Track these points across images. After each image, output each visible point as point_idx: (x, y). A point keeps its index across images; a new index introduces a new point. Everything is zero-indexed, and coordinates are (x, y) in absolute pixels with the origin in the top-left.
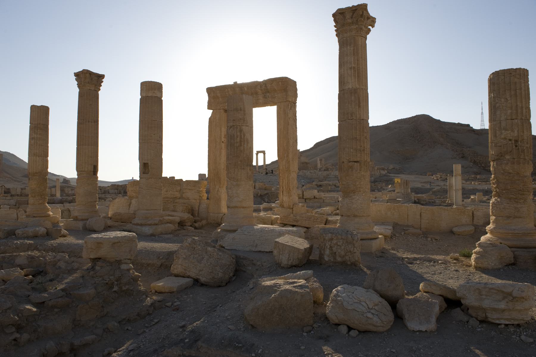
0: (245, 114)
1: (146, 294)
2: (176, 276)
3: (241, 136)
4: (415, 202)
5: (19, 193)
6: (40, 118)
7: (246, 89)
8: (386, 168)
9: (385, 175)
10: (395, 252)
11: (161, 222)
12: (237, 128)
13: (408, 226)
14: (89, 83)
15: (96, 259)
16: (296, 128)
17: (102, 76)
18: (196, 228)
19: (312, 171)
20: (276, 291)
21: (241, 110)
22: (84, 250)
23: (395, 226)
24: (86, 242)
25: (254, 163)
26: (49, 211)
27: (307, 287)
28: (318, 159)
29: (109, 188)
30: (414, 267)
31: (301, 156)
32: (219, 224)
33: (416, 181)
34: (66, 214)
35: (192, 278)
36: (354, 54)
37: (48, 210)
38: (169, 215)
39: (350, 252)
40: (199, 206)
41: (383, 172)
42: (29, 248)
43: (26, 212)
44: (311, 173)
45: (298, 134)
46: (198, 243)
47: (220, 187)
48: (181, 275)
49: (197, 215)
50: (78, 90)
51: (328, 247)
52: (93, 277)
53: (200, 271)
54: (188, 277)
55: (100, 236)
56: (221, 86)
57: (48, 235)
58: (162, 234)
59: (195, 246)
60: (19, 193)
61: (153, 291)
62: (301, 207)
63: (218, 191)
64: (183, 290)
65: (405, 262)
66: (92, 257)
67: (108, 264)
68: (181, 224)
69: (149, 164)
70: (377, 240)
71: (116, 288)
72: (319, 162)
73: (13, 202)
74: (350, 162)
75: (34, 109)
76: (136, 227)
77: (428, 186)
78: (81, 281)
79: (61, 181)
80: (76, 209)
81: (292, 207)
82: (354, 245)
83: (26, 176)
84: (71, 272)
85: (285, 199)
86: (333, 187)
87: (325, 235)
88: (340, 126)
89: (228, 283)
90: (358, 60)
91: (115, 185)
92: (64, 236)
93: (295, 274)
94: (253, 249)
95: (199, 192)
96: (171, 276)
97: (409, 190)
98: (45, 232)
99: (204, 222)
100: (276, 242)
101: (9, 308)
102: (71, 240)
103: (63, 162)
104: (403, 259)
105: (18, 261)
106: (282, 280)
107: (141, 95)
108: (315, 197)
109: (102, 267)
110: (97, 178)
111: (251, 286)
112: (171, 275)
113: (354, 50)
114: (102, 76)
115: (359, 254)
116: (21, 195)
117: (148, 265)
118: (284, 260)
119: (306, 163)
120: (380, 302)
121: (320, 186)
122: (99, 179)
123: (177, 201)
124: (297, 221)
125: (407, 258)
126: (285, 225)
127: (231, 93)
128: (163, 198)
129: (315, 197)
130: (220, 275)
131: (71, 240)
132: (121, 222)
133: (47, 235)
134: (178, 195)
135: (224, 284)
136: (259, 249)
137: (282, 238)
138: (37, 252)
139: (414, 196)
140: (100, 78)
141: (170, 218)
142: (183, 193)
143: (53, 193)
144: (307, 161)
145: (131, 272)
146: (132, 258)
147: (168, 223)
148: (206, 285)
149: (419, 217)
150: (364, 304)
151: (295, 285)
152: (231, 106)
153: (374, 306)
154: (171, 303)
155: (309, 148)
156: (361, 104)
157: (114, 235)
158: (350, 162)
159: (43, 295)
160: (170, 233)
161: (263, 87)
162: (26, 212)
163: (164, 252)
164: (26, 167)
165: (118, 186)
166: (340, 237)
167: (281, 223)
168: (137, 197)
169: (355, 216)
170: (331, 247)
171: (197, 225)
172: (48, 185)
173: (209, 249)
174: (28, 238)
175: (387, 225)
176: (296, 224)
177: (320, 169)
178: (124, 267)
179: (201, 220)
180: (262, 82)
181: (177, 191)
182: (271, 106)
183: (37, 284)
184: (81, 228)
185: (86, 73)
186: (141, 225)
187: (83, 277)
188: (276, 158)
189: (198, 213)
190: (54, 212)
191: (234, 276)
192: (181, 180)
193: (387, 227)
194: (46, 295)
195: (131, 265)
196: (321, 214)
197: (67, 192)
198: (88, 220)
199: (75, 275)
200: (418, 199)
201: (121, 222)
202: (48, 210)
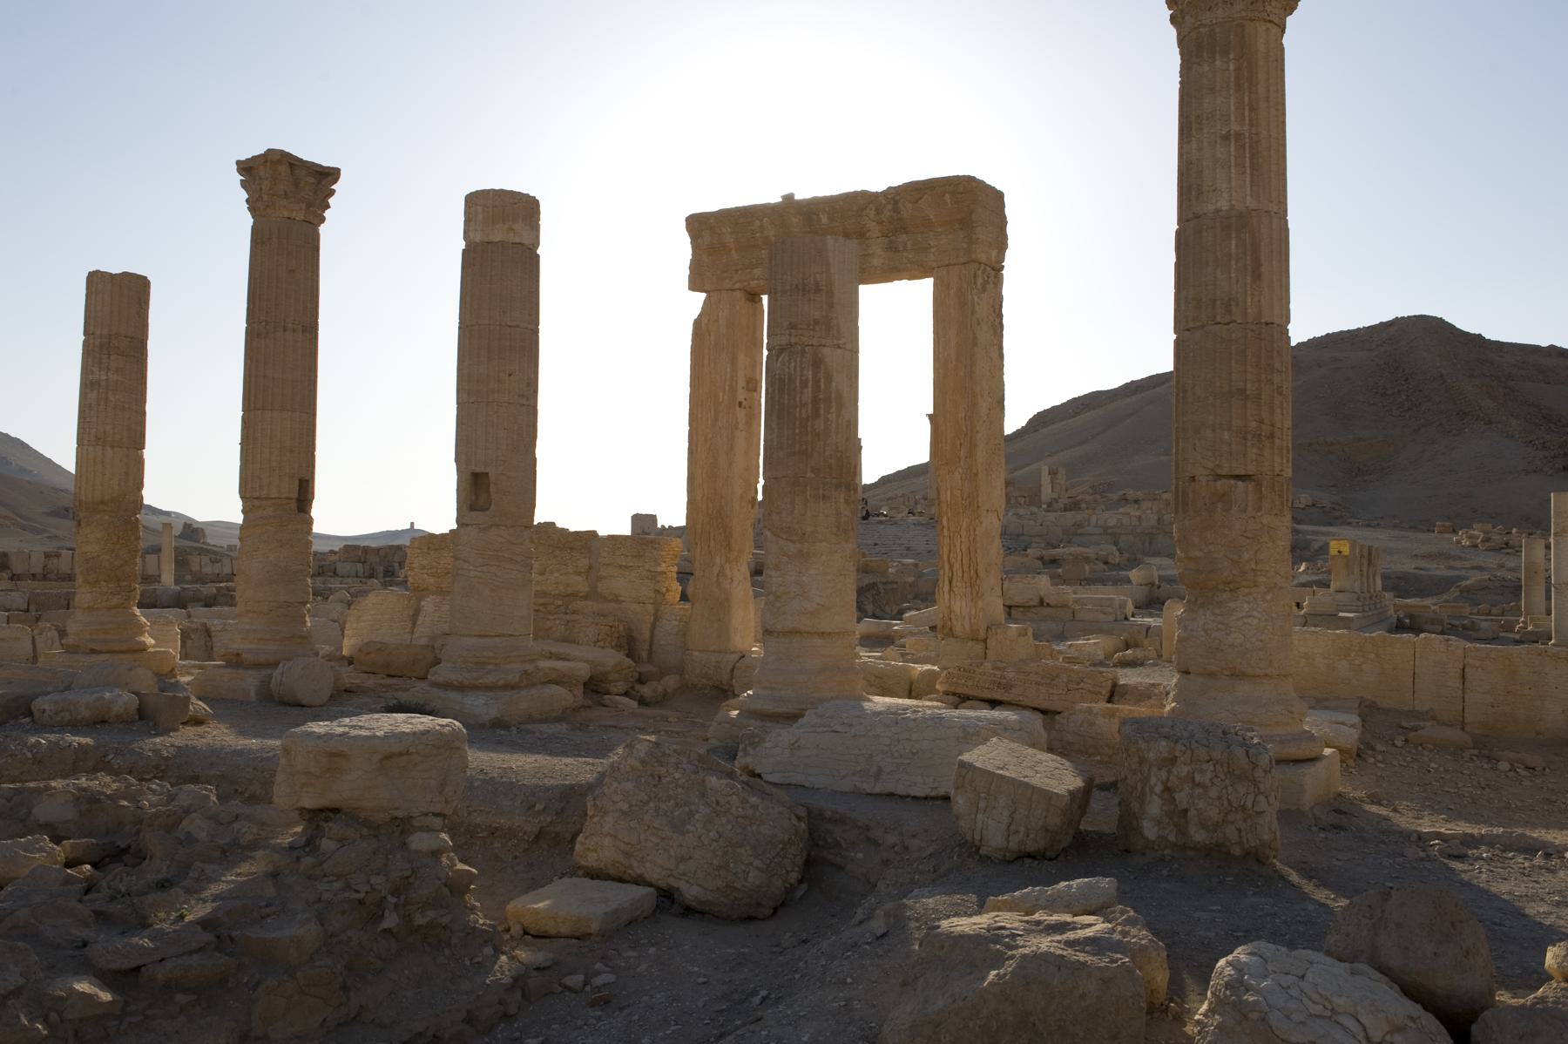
0: (831, 306)
1: (494, 941)
2: (594, 875)
3: (817, 382)
4: (1400, 627)
5: (39, 570)
6: (117, 320)
7: (824, 219)
10: (1384, 812)
11: (529, 680)
12: (803, 352)
13: (1413, 714)
14: (286, 196)
15: (321, 810)
16: (1001, 356)
17: (332, 174)
18: (642, 702)
19: (1021, 511)
20: (999, 960)
21: (818, 290)
22: (280, 777)
23: (1368, 711)
24: (286, 750)
26: (142, 633)
27: (1118, 947)
28: (1045, 470)
29: (334, 558)
30: (1478, 872)
32: (724, 693)
33: (1402, 552)
34: (199, 642)
35: (651, 885)
36: (1238, 87)
37: (140, 629)
38: (559, 658)
39: (1244, 808)
40: (653, 626)
42: (80, 762)
43: (63, 633)
44: (1019, 516)
45: (1006, 378)
46: (673, 760)
47: (728, 560)
48: (612, 871)
49: (645, 655)
50: (248, 221)
51: (1158, 789)
52: (310, 878)
53: (682, 859)
54: (639, 881)
55: (338, 727)
56: (737, 210)
57: (145, 718)
58: (530, 719)
59: (663, 771)
60: (39, 570)
61: (516, 930)
62: (1015, 639)
63: (721, 573)
64: (623, 928)
65: (1435, 852)
66: (308, 802)
67: (365, 832)
68: (595, 687)
69: (492, 478)
70: (1319, 765)
71: (391, 921)
72: (1046, 479)
73: (17, 599)
74: (1219, 477)
75: (98, 283)
76: (441, 693)
77: (1439, 570)
78: (270, 891)
79: (177, 530)
80: (235, 629)
81: (982, 635)
82: (1256, 783)
83: (63, 512)
84: (231, 853)
85: (959, 605)
86: (1101, 566)
87: (1144, 746)
88: (1178, 344)
89: (781, 906)
90: (1252, 109)
91: (356, 547)
92: (198, 722)
93: (1050, 890)
94: (867, 787)
95: (654, 576)
96: (572, 874)
97: (1379, 582)
98: (134, 707)
99: (671, 682)
100: (963, 764)
101: (16, 992)
102: (219, 736)
103: (193, 470)
104: (1421, 838)
105: (45, 811)
106: (1015, 916)
107: (466, 237)
108: (1042, 601)
109: (342, 841)
110: (310, 522)
111: (878, 925)
112: (576, 871)
113: (1238, 69)
114: (332, 174)
115: (1275, 822)
116: (45, 577)
117: (493, 832)
118: (994, 830)
120: (1412, 1019)
121: (1054, 562)
122: (316, 529)
123: (580, 604)
124: (1008, 687)
125: (1438, 835)
126: (961, 700)
127: (771, 233)
128: (537, 594)
129: (1042, 601)
130: (754, 878)
131: (219, 736)
132: (391, 678)
133: (141, 718)
134: (580, 584)
135: (768, 912)
136: (890, 788)
137: (981, 749)
138: (108, 779)
139: (1393, 605)
140: (323, 179)
141: (559, 665)
142: (600, 578)
143: (152, 570)
145: (444, 860)
146: (449, 812)
147: (550, 682)
148: (702, 913)
149: (1458, 684)
150: (1350, 1023)
151: (1071, 935)
152: (776, 280)
153: (1390, 1032)
154: (581, 978)
156: (1264, 269)
157: (387, 728)
158: (1219, 477)
159: (135, 940)
160: (558, 719)
161: (887, 213)
162: (63, 633)
163: (547, 789)
164: (71, 487)
165: (366, 550)
166: (1202, 753)
167: (947, 693)
168: (440, 592)
169: (1238, 675)
170: (1167, 789)
171: (646, 690)
172: (142, 545)
173: (713, 781)
174: (75, 726)
175: (1335, 709)
176: (1005, 698)
177: (1050, 505)
178: (419, 842)
179: (663, 673)
180: (884, 193)
181: (578, 573)
182: (910, 279)
183: (113, 899)
184: (253, 694)
185: (279, 162)
186: (461, 688)
187: (275, 875)
189: (650, 651)
190: (158, 636)
191: (800, 882)
192: (593, 534)
193: (1342, 717)
194: (147, 943)
195: (444, 836)
196: (1070, 660)
197: (195, 567)
198: (275, 665)
199: (245, 868)
200: (1412, 617)
201: (391, 678)
202: (140, 629)
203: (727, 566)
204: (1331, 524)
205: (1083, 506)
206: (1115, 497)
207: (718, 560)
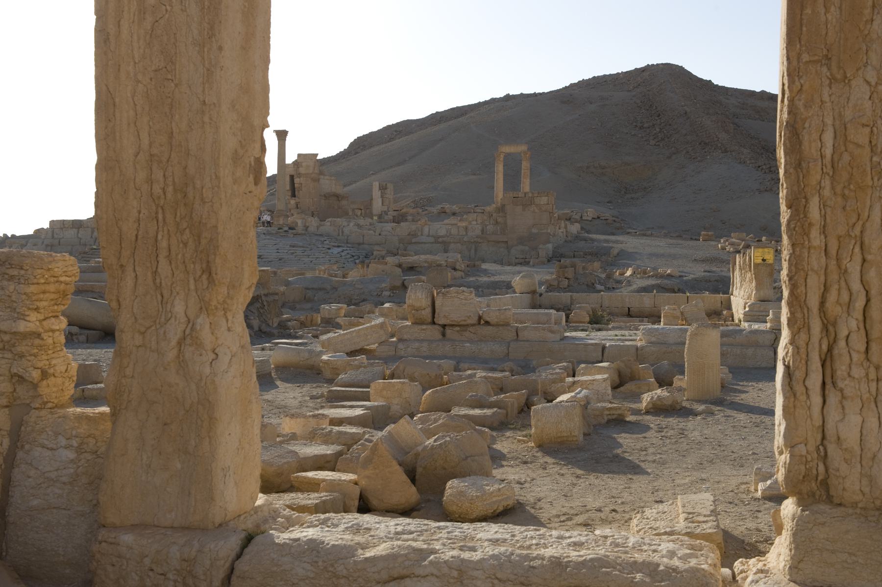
8: (578, 217)
9: (577, 238)
19: (361, 222)
25: (272, 168)
28: (376, 185)
31: (321, 173)
41: (575, 228)
44: (358, 225)
47: (205, 307)
63: (190, 337)
72: (376, 193)
119: (338, 197)
144: (339, 190)
155: (334, 154)
177: (380, 216)
188: (276, 172)
203: (203, 321)
204: (613, 234)
205: (410, 218)
206: (435, 210)
207: (179, 308)
